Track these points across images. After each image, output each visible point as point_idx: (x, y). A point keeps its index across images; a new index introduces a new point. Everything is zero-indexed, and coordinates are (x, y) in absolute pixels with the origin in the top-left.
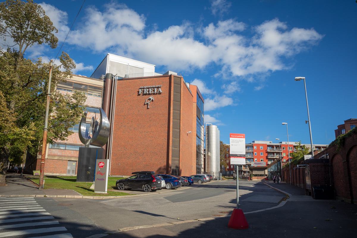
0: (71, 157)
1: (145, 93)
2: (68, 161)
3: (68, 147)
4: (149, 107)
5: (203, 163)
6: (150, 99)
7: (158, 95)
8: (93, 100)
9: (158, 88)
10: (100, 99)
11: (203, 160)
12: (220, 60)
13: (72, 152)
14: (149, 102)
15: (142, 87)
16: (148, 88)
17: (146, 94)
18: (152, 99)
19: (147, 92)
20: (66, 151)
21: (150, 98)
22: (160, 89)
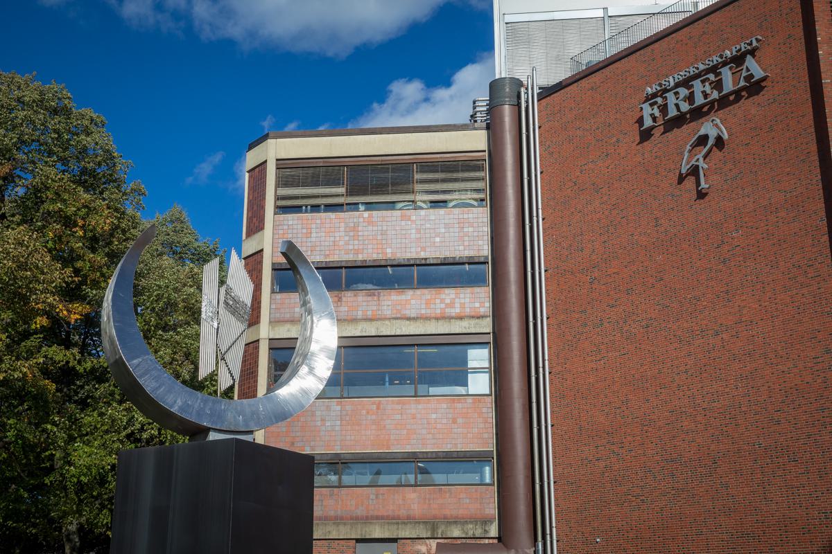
0: (368, 520)
1: (672, 112)
2: (358, 541)
3: (348, 474)
4: (703, 185)
6: (703, 140)
7: (748, 106)
8: (447, 226)
9: (738, 60)
10: (480, 217)
13: (372, 497)
15: (656, 88)
17: (679, 121)
18: (713, 133)
20: (344, 491)
21: (702, 132)
22: (750, 62)
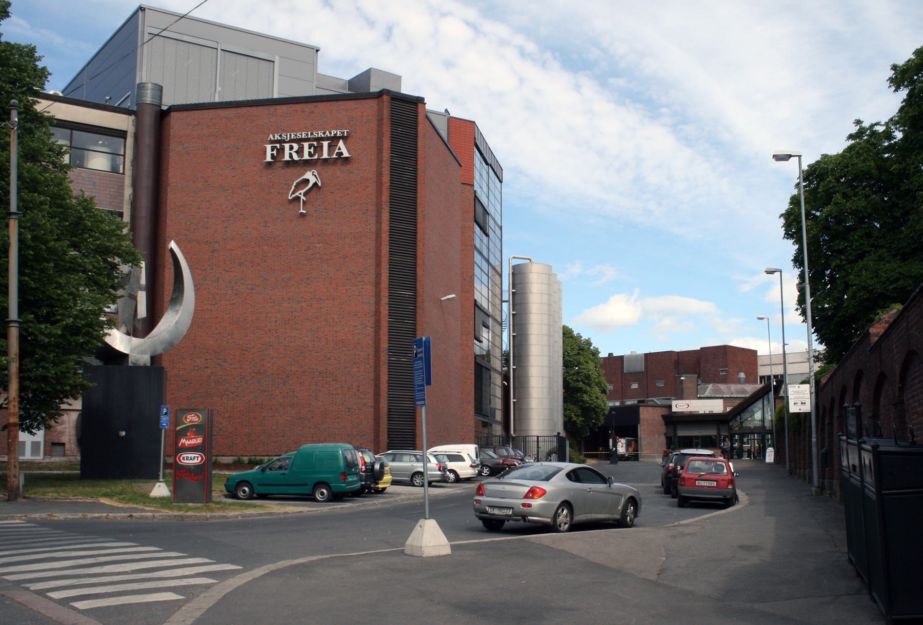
5: (498, 404)
9: (334, 140)
11: (498, 392)
12: (50, 74)
14: (302, 192)
15: (277, 137)
16: (299, 141)
19: (296, 157)
